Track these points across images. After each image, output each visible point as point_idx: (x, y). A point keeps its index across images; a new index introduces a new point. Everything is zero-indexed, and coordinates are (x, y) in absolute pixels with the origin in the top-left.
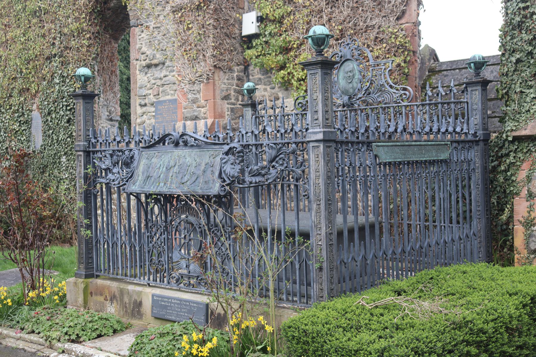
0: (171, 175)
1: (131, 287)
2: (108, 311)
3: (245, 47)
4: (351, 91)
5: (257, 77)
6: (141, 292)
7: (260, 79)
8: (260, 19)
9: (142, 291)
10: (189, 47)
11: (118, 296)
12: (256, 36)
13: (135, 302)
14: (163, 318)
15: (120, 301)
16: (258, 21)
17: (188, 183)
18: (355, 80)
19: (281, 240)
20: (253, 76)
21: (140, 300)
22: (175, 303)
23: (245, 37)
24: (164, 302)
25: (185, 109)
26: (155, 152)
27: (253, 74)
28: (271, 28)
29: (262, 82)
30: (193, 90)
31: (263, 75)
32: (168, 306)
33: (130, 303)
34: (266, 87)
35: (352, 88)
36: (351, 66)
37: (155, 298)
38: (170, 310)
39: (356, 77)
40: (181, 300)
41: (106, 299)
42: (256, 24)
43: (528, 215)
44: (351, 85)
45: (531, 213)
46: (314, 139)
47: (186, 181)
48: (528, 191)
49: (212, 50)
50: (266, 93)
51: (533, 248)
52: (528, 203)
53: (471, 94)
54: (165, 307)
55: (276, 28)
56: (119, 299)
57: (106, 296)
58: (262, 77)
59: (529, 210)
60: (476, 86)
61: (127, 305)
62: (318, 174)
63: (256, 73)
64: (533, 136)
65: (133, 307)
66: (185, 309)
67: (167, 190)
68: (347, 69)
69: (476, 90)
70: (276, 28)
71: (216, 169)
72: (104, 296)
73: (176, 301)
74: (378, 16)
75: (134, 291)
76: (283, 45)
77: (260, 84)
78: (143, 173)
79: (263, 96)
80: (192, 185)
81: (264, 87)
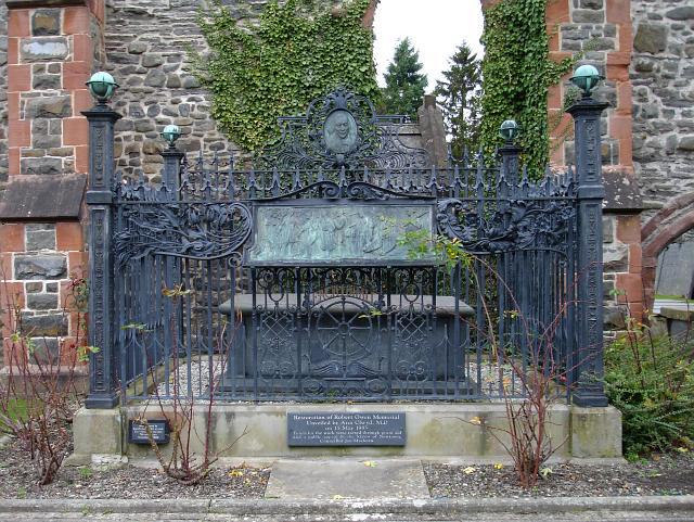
14: (317, 444)
22: (340, 421)
54: (321, 429)
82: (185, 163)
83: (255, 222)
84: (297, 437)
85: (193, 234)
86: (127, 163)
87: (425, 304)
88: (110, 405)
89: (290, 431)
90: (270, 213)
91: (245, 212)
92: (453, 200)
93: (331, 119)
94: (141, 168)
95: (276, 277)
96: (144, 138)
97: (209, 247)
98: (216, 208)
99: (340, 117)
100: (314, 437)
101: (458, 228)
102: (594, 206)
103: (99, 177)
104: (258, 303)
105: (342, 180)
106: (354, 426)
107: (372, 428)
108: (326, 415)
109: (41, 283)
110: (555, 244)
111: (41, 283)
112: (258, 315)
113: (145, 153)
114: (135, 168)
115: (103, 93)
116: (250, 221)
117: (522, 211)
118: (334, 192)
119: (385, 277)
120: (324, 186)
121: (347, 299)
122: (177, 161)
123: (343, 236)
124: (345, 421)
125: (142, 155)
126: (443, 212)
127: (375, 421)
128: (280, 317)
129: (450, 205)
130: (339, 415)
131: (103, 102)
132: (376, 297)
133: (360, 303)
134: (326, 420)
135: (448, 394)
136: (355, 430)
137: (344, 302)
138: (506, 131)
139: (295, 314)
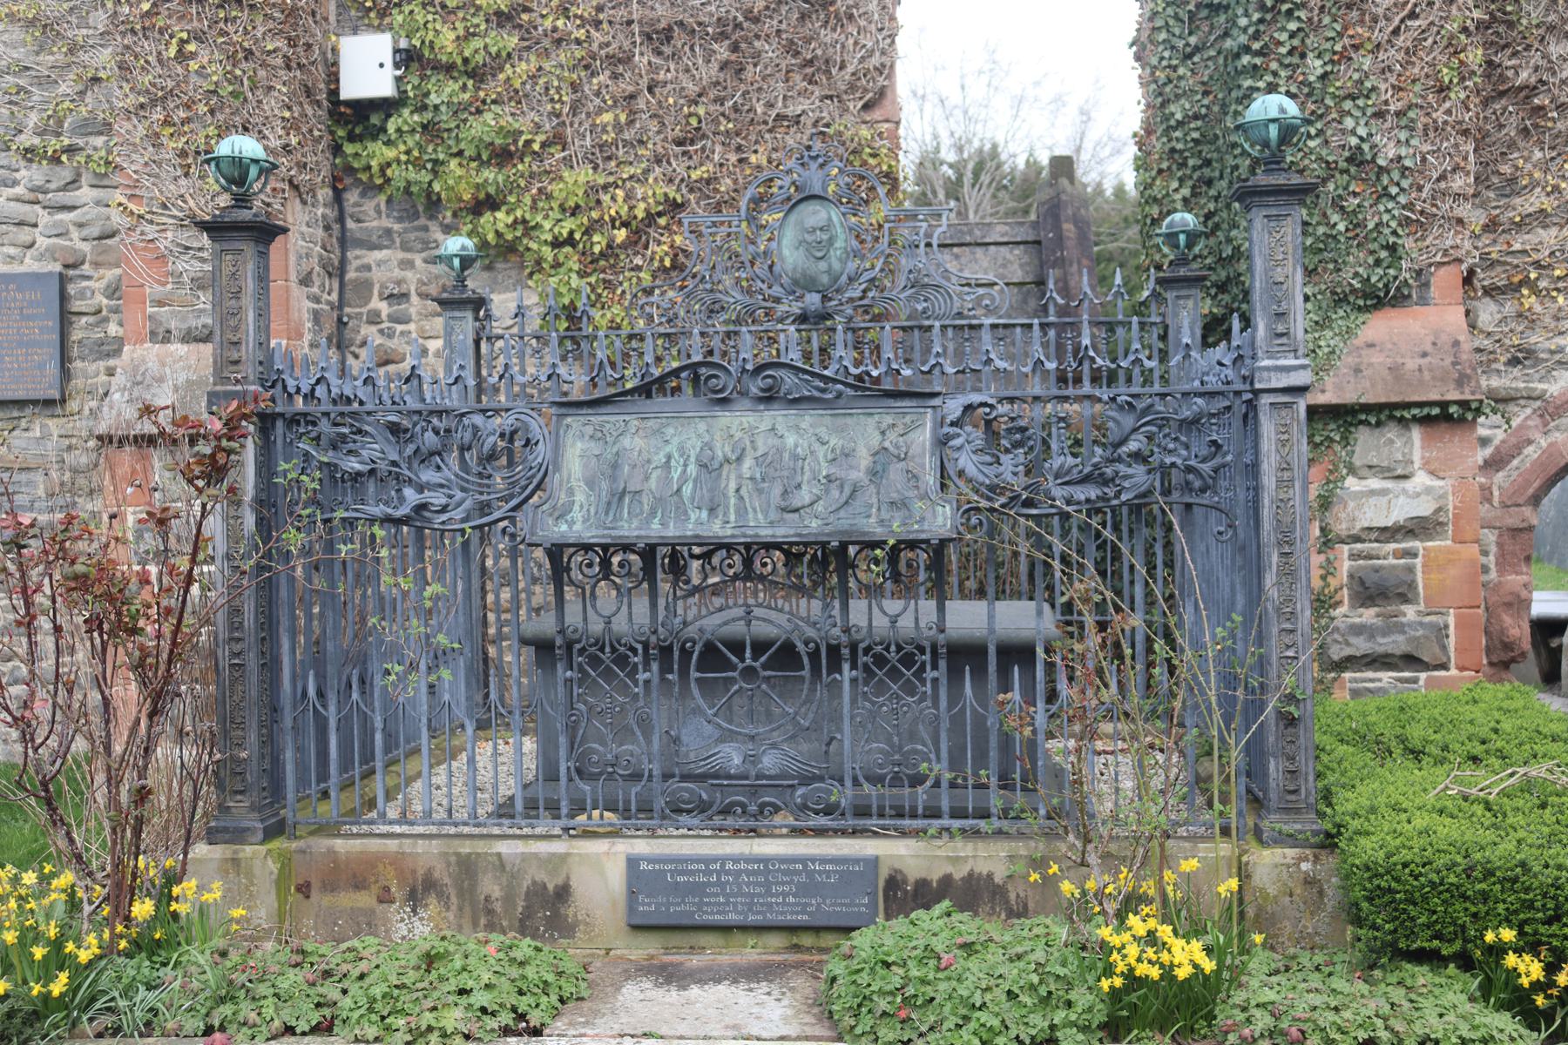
0: (733, 486)
1: (503, 847)
2: (397, 938)
3: (341, 133)
4: (825, 279)
5: (375, 223)
6: (564, 858)
7: (388, 232)
8: (407, 58)
9: (568, 855)
10: (182, 114)
11: (447, 880)
12: (385, 106)
13: (538, 890)
14: (685, 922)
15: (460, 894)
16: (397, 66)
17: (819, 507)
18: (836, 254)
19: (820, 676)
20: (359, 221)
21: (560, 881)
22: (738, 873)
23: (348, 103)
24: (692, 873)
25: (160, 304)
26: (627, 418)
27: (362, 217)
28: (444, 92)
29: (393, 242)
30: (200, 249)
31: (400, 220)
32: (709, 884)
33: (508, 899)
34: (409, 256)
35: (829, 271)
36: (823, 215)
37: (644, 866)
38: (717, 895)
39: (839, 244)
40: (765, 860)
41: (385, 898)
42: (389, 73)
43: (1321, 583)
44: (823, 265)
45: (1330, 579)
46: (1280, 385)
47: (807, 500)
48: (1322, 529)
49: (281, 132)
50: (409, 274)
51: (1336, 658)
52: (1322, 557)
53: (1175, 305)
54: (698, 889)
55: (464, 88)
56: (453, 892)
57: (387, 889)
58: (396, 227)
59: (1322, 572)
60: (1189, 287)
61: (498, 907)
62: (1286, 475)
63: (372, 213)
64: (1344, 406)
65: (526, 908)
66: (783, 883)
67: (729, 532)
68: (811, 221)
69: (1188, 297)
70: (464, 88)
71: (923, 466)
72: (375, 889)
73: (743, 866)
74: (803, 93)
75: (525, 857)
76: (498, 141)
77: (387, 247)
78: (590, 483)
79: (399, 283)
80: (842, 513)
81: (401, 255)
82: (488, 316)
83: (557, 449)
84: (648, 908)
85: (428, 475)
86: (384, 315)
87: (922, 624)
88: (260, 835)
89: (632, 894)
90: (589, 430)
91: (536, 427)
92: (976, 398)
93: (793, 218)
94: (412, 327)
95: (606, 564)
96: (418, 262)
97: (459, 505)
98: (478, 419)
99: (814, 214)
100: (681, 909)
101: (988, 459)
102: (1287, 405)
103: (235, 356)
104: (568, 620)
105: (139, 378)
106: (767, 885)
107: (806, 890)
108: (708, 860)
109: (803, 668)
110: (1203, 490)
111: (803, 668)
112: (569, 646)
113: (420, 295)
114: (399, 328)
115: (241, 181)
116: (542, 452)
117: (1128, 421)
118: (721, 383)
119: (826, 562)
120: (703, 370)
121: (757, 612)
122: (469, 315)
123: (740, 477)
124: (749, 873)
125: (414, 299)
126: (952, 424)
127: (811, 874)
128: (614, 650)
129: (969, 408)
130: (736, 860)
131: (242, 201)
132: (816, 605)
133: (782, 619)
134: (708, 873)
135: (953, 816)
136: (769, 893)
137: (748, 617)
138: (1171, 237)
139: (646, 646)
